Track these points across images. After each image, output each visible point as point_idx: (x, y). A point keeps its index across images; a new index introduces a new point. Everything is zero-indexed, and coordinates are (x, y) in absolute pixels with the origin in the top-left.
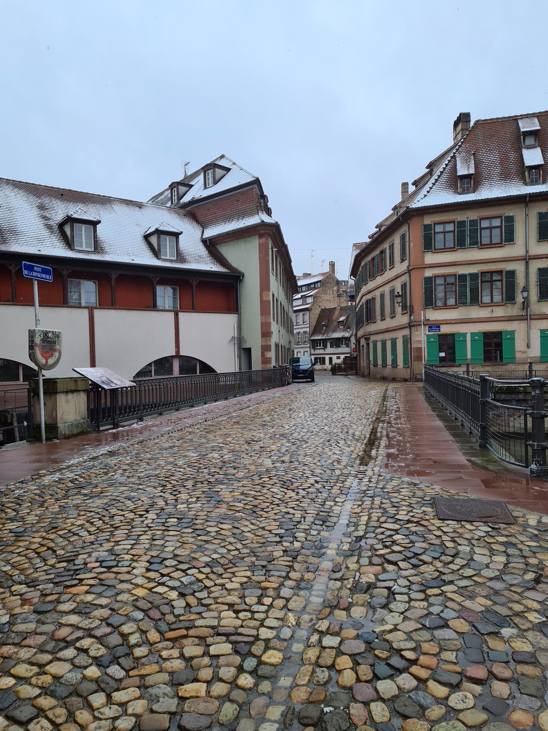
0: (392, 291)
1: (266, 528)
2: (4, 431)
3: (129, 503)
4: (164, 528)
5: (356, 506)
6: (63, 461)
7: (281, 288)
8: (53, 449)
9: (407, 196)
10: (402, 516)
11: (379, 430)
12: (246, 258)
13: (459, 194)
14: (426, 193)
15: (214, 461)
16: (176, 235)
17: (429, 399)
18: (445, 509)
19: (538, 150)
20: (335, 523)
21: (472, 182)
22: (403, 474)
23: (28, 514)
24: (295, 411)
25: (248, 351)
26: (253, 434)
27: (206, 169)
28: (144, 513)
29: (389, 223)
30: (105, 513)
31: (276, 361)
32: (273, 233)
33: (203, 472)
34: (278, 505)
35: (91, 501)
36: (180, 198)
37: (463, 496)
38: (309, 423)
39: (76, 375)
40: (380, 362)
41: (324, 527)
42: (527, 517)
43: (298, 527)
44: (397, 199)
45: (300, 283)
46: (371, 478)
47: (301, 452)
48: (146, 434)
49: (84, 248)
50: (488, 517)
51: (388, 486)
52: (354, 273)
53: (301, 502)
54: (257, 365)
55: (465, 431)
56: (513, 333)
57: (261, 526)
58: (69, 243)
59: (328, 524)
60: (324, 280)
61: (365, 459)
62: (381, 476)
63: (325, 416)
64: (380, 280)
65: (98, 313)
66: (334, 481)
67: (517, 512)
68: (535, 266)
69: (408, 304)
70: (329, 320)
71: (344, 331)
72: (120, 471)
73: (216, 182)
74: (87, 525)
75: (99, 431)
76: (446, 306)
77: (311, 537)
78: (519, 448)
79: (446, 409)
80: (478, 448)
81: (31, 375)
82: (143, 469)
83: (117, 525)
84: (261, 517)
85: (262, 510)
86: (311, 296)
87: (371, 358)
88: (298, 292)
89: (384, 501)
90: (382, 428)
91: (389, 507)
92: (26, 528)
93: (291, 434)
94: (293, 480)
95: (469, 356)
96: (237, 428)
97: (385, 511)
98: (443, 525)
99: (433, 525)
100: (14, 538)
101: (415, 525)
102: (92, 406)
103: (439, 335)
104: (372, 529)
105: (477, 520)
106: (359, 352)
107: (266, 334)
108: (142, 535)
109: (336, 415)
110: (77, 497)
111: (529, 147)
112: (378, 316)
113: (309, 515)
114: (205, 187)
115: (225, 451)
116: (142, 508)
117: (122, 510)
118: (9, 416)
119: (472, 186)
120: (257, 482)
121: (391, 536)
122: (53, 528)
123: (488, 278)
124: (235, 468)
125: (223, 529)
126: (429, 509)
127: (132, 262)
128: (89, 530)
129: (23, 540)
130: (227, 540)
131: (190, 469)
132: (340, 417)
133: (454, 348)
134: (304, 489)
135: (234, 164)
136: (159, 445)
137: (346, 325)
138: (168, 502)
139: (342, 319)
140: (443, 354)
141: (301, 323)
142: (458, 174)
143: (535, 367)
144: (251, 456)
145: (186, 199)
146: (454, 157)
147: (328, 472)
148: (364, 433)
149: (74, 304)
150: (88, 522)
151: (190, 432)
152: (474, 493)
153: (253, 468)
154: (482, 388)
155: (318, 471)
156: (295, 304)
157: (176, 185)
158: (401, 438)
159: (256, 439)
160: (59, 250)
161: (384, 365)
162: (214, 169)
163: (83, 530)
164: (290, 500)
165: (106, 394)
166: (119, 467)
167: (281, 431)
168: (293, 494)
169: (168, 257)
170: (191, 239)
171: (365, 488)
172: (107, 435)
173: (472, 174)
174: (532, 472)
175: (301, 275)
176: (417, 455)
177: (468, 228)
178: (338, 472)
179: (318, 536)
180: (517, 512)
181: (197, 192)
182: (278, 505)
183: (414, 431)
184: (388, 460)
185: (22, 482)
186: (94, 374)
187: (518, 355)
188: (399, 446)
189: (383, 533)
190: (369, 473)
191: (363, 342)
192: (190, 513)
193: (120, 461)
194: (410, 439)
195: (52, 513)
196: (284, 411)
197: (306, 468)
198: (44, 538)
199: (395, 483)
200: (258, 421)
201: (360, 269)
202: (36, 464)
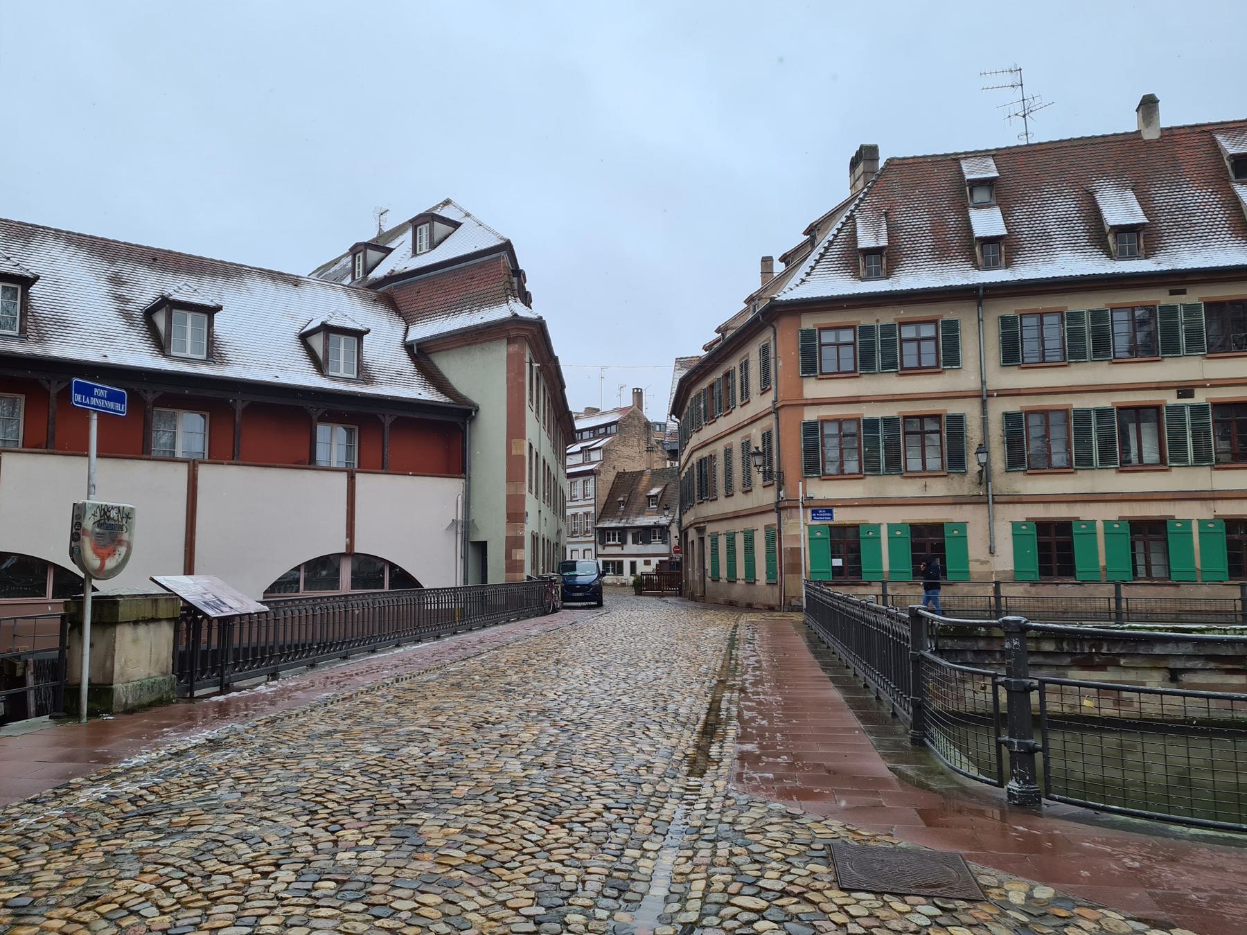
0: (746, 445)
1: (509, 904)
2: (8, 696)
3: (242, 847)
4: (309, 901)
5: (683, 860)
6: (120, 760)
7: (544, 434)
8: (100, 735)
9: (771, 280)
10: (771, 881)
11: (724, 705)
12: (483, 379)
13: (862, 280)
14: (803, 276)
15: (412, 763)
16: (359, 335)
17: (815, 645)
18: (855, 870)
19: (996, 212)
20: (642, 895)
21: (884, 261)
22: (771, 795)
23: (42, 867)
24: (566, 665)
25: (482, 547)
26: (488, 709)
27: (416, 222)
28: (272, 868)
29: (739, 324)
30: (194, 868)
31: (533, 567)
32: (532, 337)
33: (388, 786)
34: (532, 855)
35: (168, 842)
36: (368, 271)
37: (884, 842)
38: (592, 688)
39: (157, 590)
40: (723, 573)
41: (621, 902)
42: (1006, 887)
43: (570, 901)
44: (754, 284)
45: (579, 425)
46: (710, 802)
47: (578, 747)
48: (283, 704)
49: (188, 353)
50: (933, 886)
51: (743, 820)
52: (677, 409)
53: (576, 849)
54: (497, 574)
55: (884, 711)
56: (962, 526)
57: (500, 898)
58: (161, 345)
59: (628, 896)
60: (623, 420)
61: (699, 763)
62: (730, 798)
63: (623, 675)
64: (723, 424)
65: (204, 472)
66: (639, 805)
67: (989, 877)
68: (999, 408)
69: (775, 469)
70: (632, 493)
71: (657, 513)
72: (229, 781)
73: (433, 245)
74: (158, 893)
75: (192, 698)
76: (842, 475)
77: (595, 922)
78: (984, 743)
79: (848, 667)
80: (909, 745)
81: (69, 585)
82: (274, 779)
83: (216, 894)
84: (501, 880)
85: (502, 864)
86: (599, 448)
87: (708, 566)
88: (575, 442)
89: (736, 850)
90: (730, 702)
91: (745, 863)
92: (36, 899)
93: (560, 710)
94: (563, 804)
95: (886, 567)
96: (457, 696)
97: (738, 871)
98: (848, 901)
99: (830, 900)
100: (11, 919)
101: (796, 900)
102: (182, 647)
103: (831, 527)
104: (714, 908)
105: (914, 891)
106: (686, 554)
107: (516, 515)
108: (265, 915)
109: (642, 675)
110: (141, 833)
111: (979, 206)
112: (721, 490)
113: (592, 877)
114: (415, 254)
115: (433, 743)
116: (268, 860)
117: (228, 863)
118: (20, 664)
119: (884, 267)
120: (494, 806)
121: (750, 923)
122: (90, 899)
123: (916, 426)
124: (451, 778)
125: (424, 905)
126: (821, 869)
127: (275, 380)
128: (161, 903)
129: (28, 924)
130: (431, 927)
131: (365, 779)
132: (651, 678)
133: (858, 550)
134: (582, 823)
135: (468, 215)
136: (305, 729)
137: (661, 503)
138: (319, 846)
139: (654, 491)
140: (838, 562)
141: (580, 496)
142: (860, 246)
143: (1005, 591)
144: (482, 753)
145: (379, 272)
146: (851, 218)
147: (630, 788)
148: (695, 709)
149: (161, 454)
150: (159, 886)
151: (367, 703)
152: (904, 838)
153: (485, 777)
154: (913, 631)
155: (609, 786)
156: (569, 462)
157: (362, 247)
158: (764, 722)
159: (492, 719)
160: (142, 357)
161: (732, 579)
162: (431, 224)
163: (149, 904)
164: (555, 845)
165: (210, 627)
166: (228, 773)
167: (540, 703)
168: (562, 833)
169: (342, 374)
170: (385, 342)
171: (698, 823)
172: (206, 706)
173: (883, 248)
174: (1011, 795)
175: (582, 410)
176: (797, 757)
177: (878, 338)
178: (647, 789)
179: (610, 921)
180: (989, 877)
181: (400, 260)
182: (532, 855)
183: (790, 708)
184: (742, 767)
185: (34, 802)
186: (189, 588)
187: (974, 568)
188: (762, 737)
189: (734, 917)
190: (707, 791)
191: (692, 535)
192: (362, 870)
193: (230, 760)
194: (781, 725)
195: (90, 867)
196: (546, 664)
197: (586, 779)
198: (70, 920)
199: (755, 813)
200: (498, 683)
201: (689, 404)
202: (66, 765)
